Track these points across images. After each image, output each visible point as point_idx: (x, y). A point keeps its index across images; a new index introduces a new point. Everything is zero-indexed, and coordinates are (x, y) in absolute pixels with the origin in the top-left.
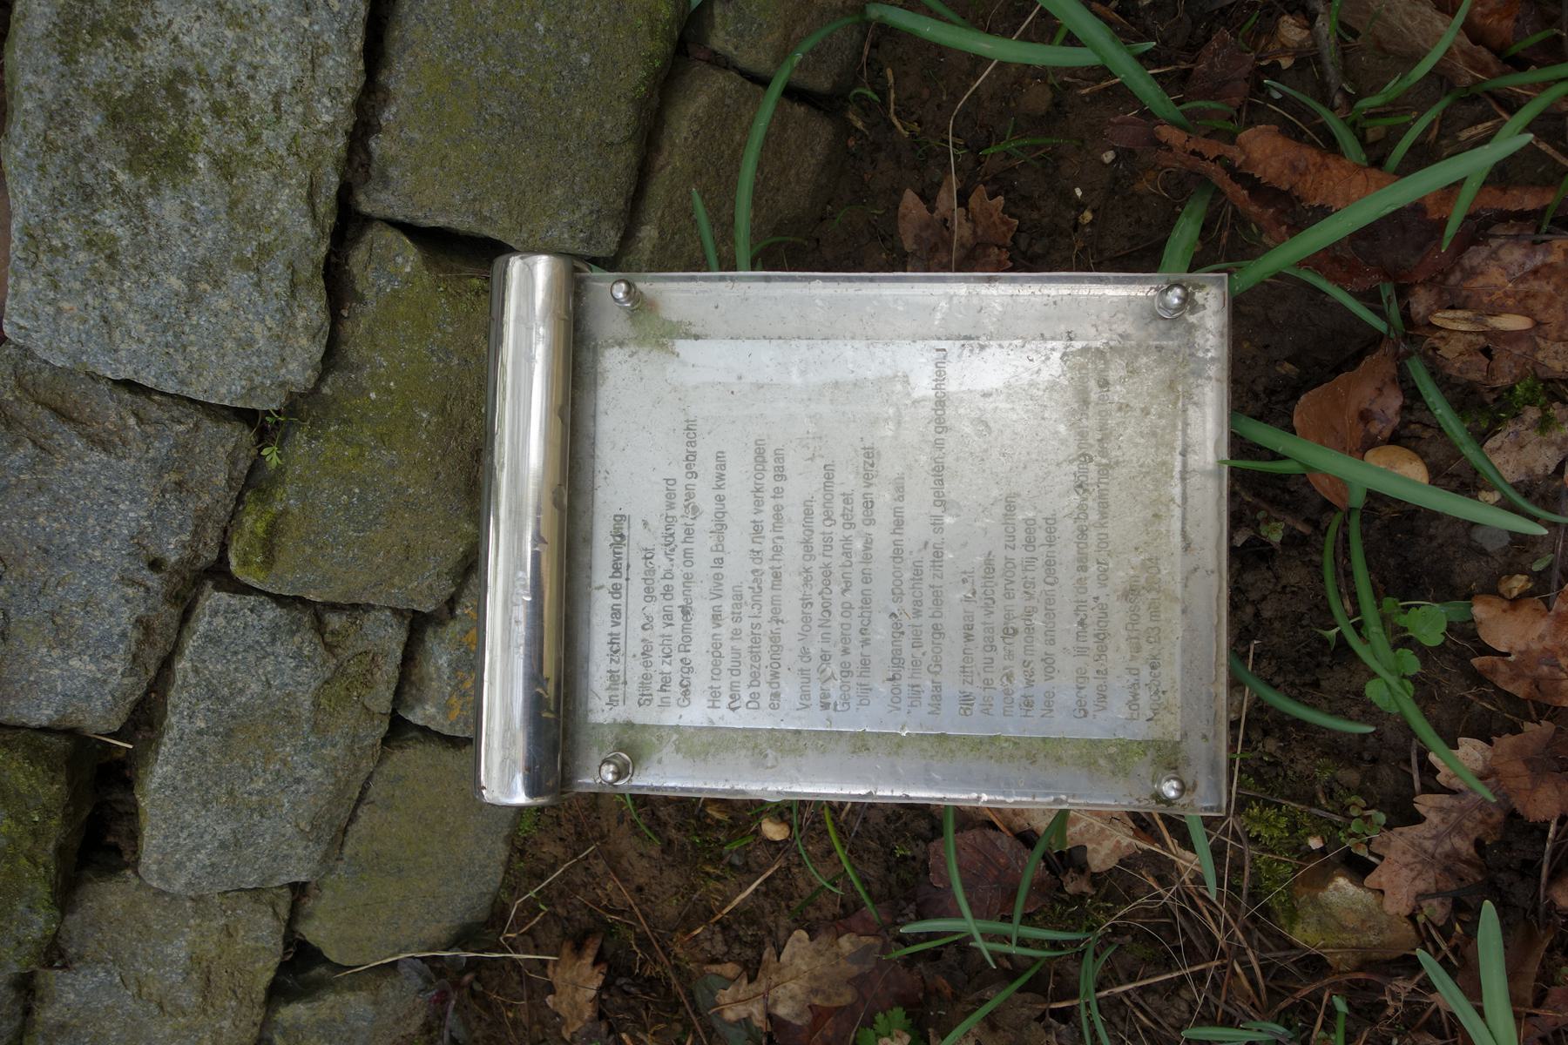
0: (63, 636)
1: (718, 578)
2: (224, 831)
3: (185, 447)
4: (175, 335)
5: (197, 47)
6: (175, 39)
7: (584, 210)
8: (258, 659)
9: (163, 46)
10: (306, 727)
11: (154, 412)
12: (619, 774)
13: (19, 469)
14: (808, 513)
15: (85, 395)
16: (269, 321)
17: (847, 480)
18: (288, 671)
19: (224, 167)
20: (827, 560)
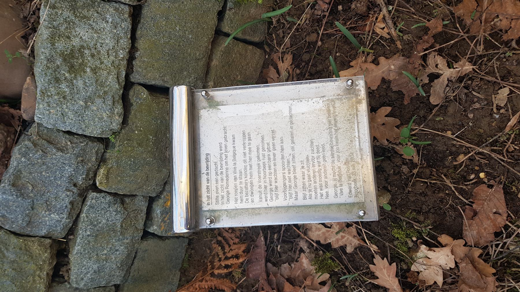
0: (49, 208)
1: (235, 168)
2: (95, 267)
3: (84, 150)
4: (82, 117)
5: (87, 39)
6: (81, 38)
7: (193, 78)
8: (105, 212)
9: (78, 40)
10: (119, 233)
11: (75, 140)
12: (211, 222)
13: (38, 159)
14: (258, 149)
15: (56, 137)
16: (107, 112)
17: (268, 139)
18: (114, 216)
19: (94, 70)
20: (264, 161)
